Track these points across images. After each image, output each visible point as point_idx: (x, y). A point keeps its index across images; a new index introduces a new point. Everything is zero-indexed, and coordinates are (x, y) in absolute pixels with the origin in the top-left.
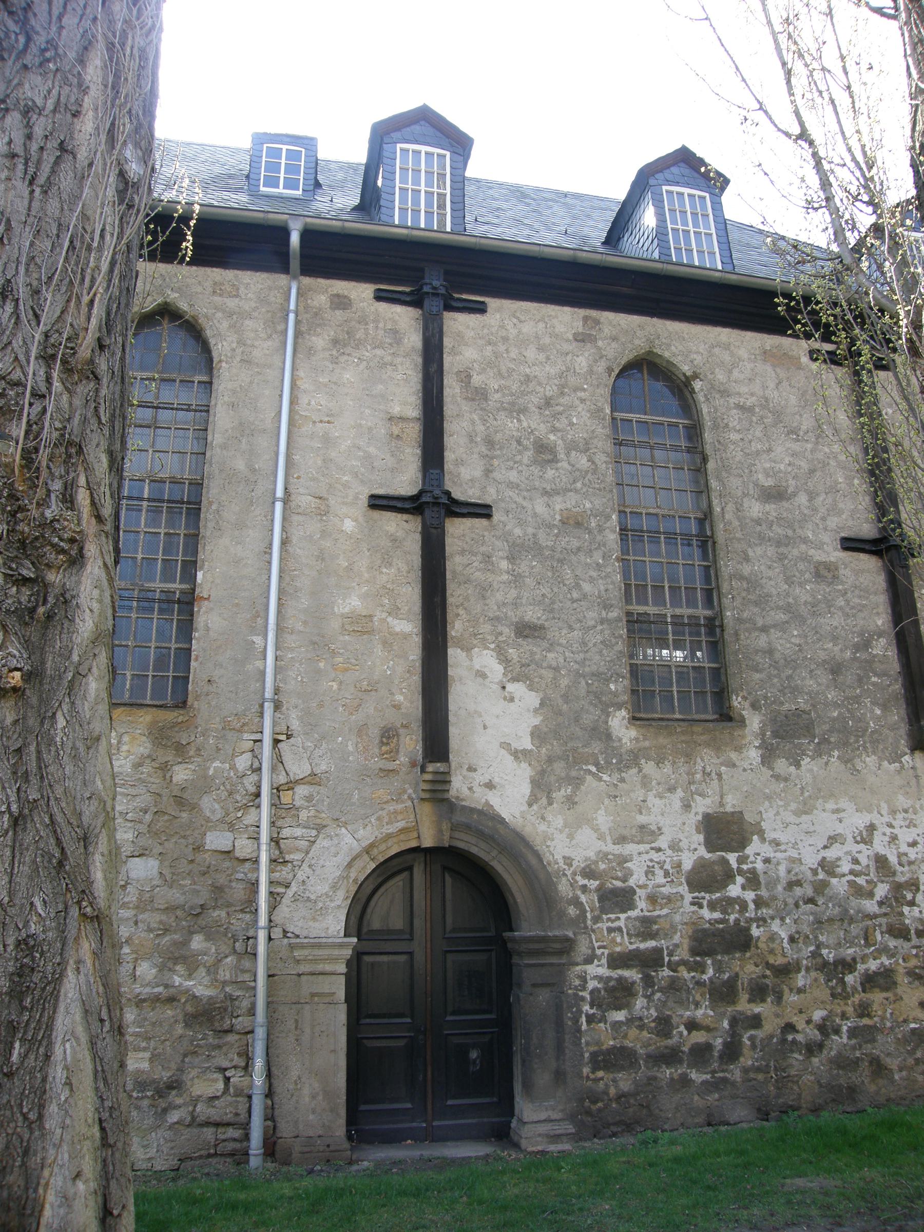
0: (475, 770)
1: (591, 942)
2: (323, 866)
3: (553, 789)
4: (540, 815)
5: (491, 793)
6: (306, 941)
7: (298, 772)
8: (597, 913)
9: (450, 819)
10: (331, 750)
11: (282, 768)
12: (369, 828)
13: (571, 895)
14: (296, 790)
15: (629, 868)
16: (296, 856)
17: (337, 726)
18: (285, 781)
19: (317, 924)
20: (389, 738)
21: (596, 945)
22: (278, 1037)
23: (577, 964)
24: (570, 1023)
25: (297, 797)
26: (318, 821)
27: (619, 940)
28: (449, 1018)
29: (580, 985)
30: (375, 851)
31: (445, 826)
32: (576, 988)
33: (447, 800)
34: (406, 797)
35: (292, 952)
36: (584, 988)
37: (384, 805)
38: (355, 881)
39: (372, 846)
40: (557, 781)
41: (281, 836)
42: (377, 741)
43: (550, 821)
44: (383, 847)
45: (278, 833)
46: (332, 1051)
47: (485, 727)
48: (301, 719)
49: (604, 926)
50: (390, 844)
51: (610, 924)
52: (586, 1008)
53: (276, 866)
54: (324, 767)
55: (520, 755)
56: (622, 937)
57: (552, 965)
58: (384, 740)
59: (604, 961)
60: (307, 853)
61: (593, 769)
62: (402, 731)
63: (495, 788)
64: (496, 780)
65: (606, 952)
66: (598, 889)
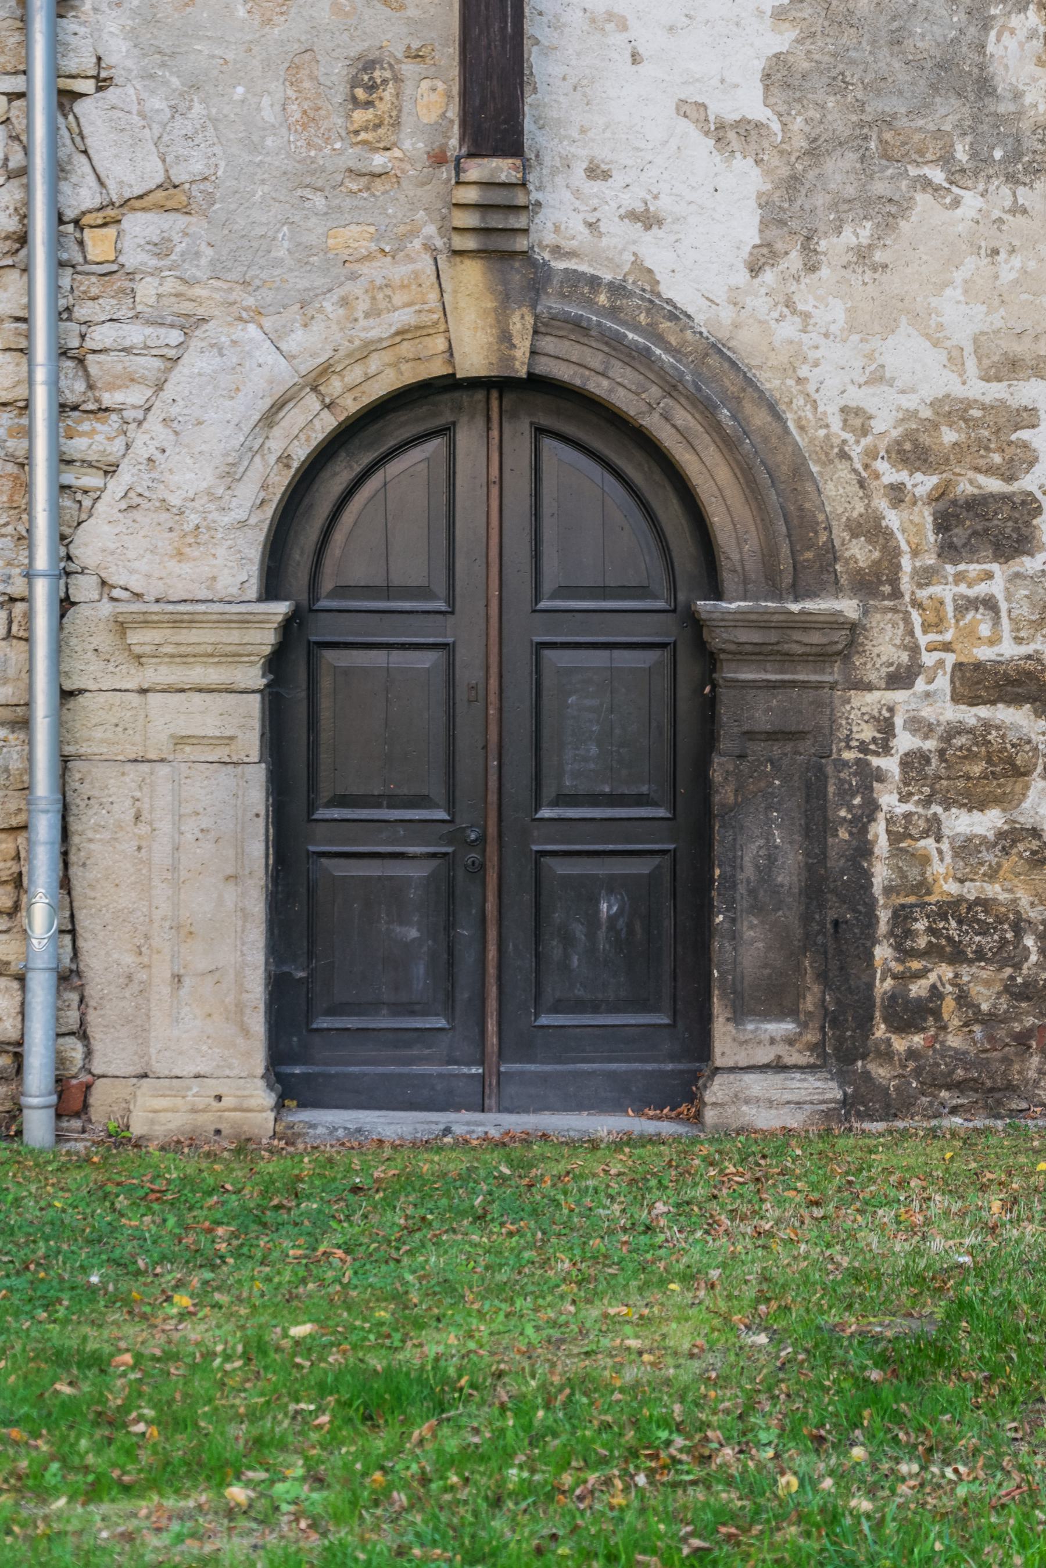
0: (606, 175)
1: (911, 633)
2: (200, 423)
3: (822, 228)
4: (782, 299)
5: (648, 237)
6: (156, 608)
7: (130, 178)
8: (930, 560)
9: (533, 307)
10: (215, 121)
11: (87, 169)
12: (317, 326)
13: (860, 508)
14: (125, 224)
15: (1025, 446)
16: (134, 396)
17: (230, 56)
18: (96, 202)
19: (186, 568)
20: (371, 88)
21: (923, 640)
22: (91, 840)
23: (869, 687)
24: (843, 834)
25: (127, 244)
26: (187, 307)
27: (985, 630)
28: (545, 813)
29: (874, 740)
30: (335, 386)
31: (520, 323)
32: (863, 748)
33: (525, 255)
34: (417, 244)
35: (123, 634)
36: (886, 749)
37: (356, 267)
38: (284, 460)
39: (326, 370)
40: (834, 206)
41: (89, 344)
42: (339, 99)
43: (806, 316)
44: (355, 374)
45: (83, 337)
46: (228, 878)
47: (636, 58)
48: (132, 35)
49: (946, 592)
50: (373, 369)
51: (962, 589)
52: (888, 799)
53: (79, 422)
54: (197, 167)
55: (731, 135)
56: (996, 621)
57: (804, 685)
58: (360, 93)
59: (943, 683)
60: (159, 387)
61: (937, 175)
62: (408, 69)
63: (660, 223)
64: (664, 205)
65: (950, 659)
66: (939, 495)
